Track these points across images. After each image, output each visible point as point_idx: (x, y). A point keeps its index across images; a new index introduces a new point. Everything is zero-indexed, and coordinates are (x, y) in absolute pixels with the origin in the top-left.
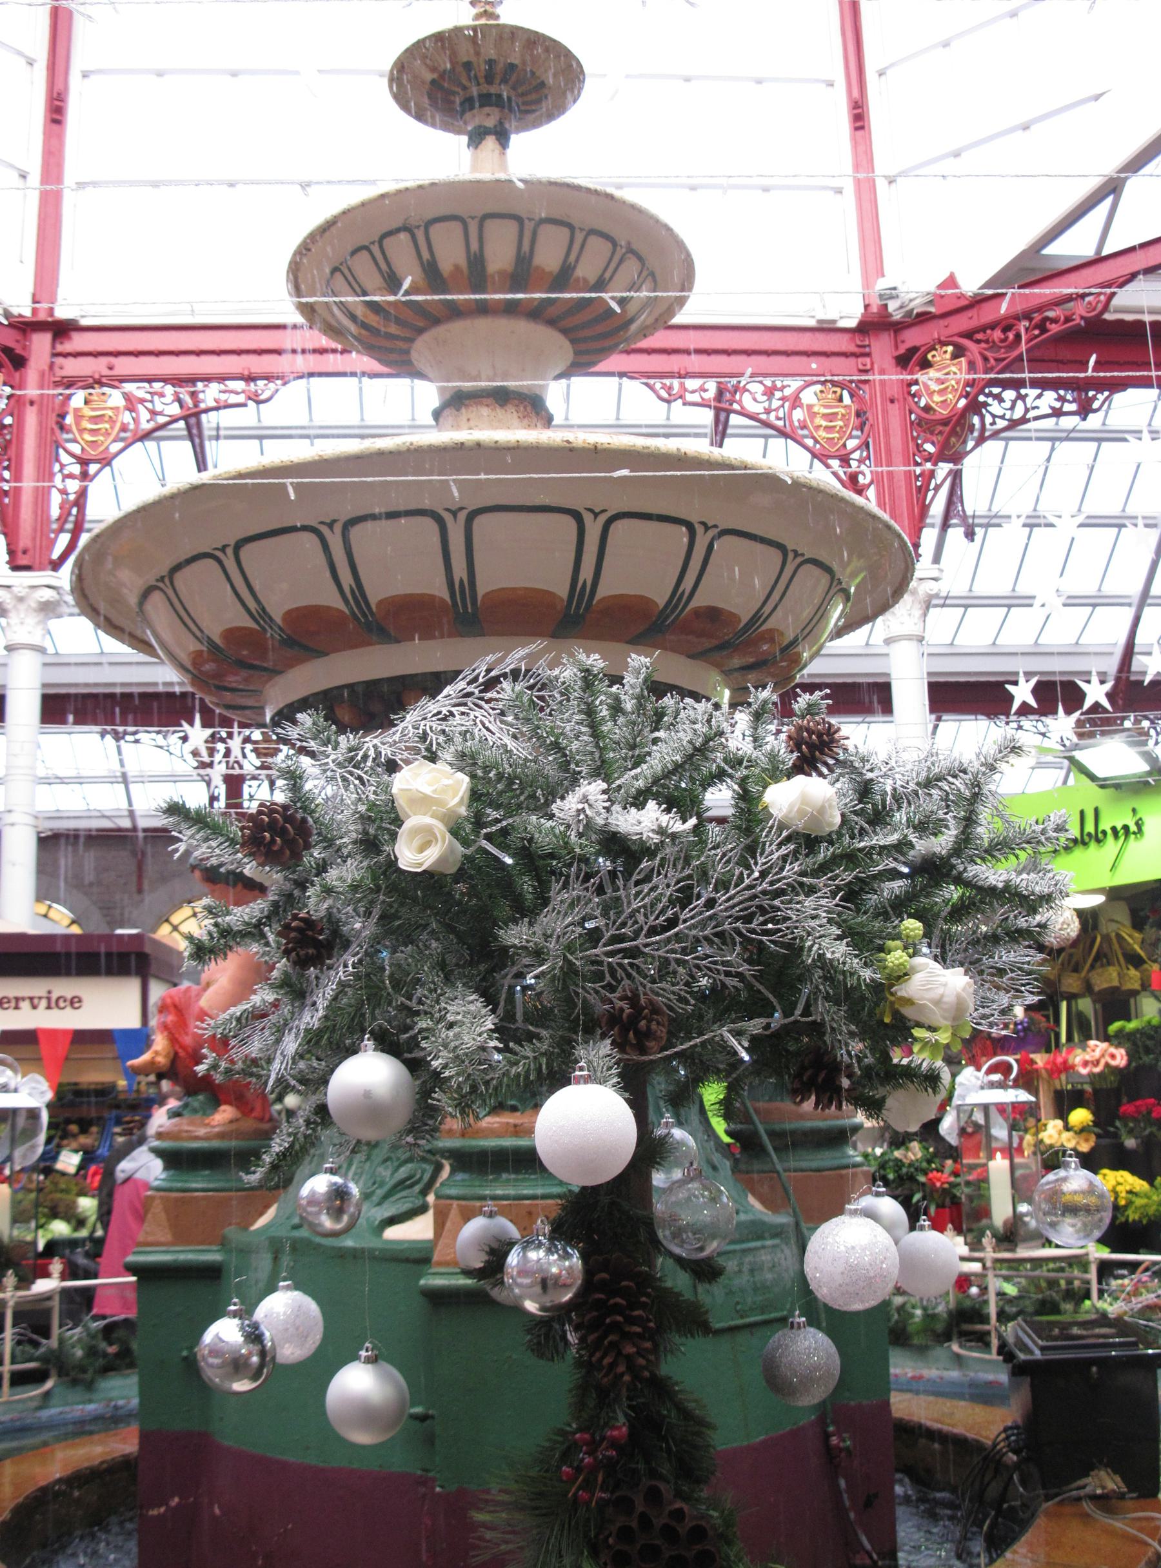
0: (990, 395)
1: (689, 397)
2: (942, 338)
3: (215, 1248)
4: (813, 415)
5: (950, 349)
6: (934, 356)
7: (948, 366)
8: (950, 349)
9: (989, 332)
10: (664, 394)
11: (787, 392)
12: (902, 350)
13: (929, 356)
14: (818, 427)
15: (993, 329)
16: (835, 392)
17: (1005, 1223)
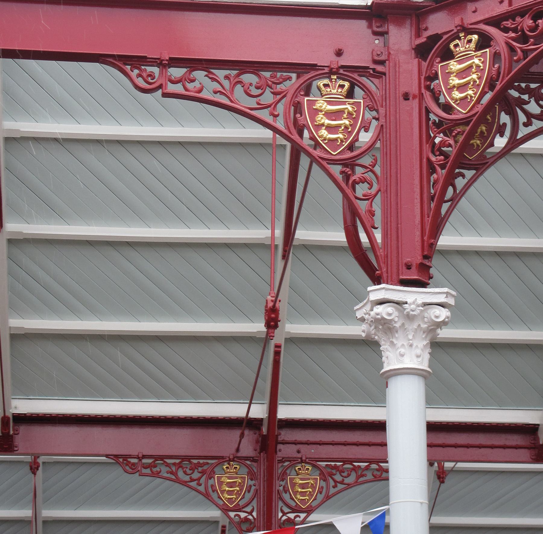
0: (527, 91)
1: (172, 88)
5: (475, 37)
6: (456, 46)
7: (472, 57)
8: (475, 37)
9: (518, 19)
10: (140, 82)
12: (422, 40)
14: (319, 127)
15: (522, 16)
16: (342, 86)
17: (355, 88)
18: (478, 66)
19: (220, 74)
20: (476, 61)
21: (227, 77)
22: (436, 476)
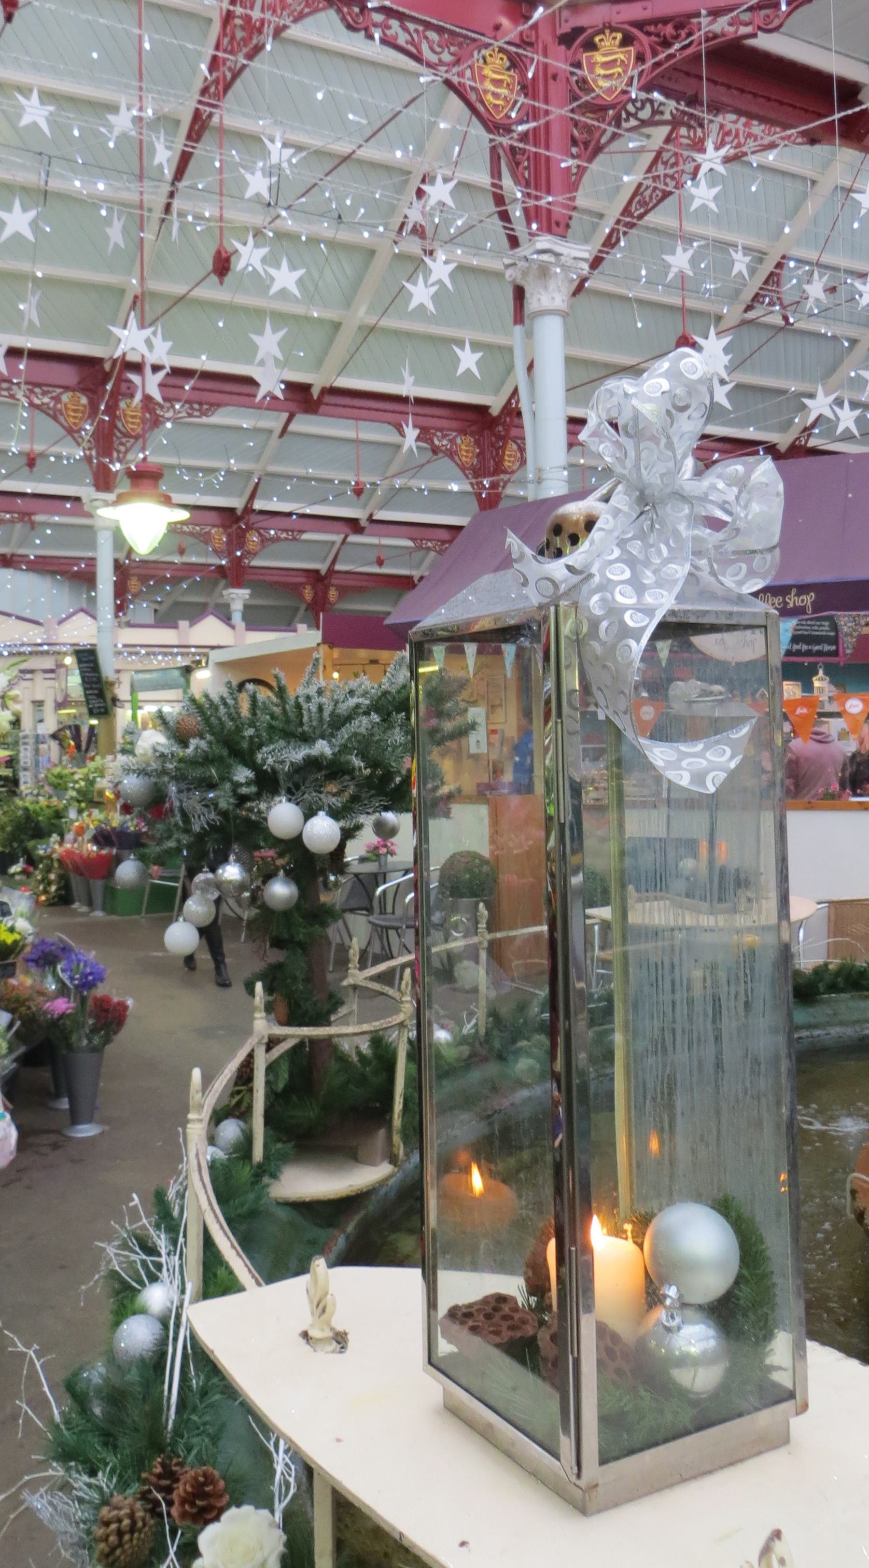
2: (613, 24)
3: (707, 938)
4: (66, 409)
8: (619, 36)
9: (660, 26)
11: (54, 394)
13: (597, 39)
18: (622, 61)
19: (411, 26)
20: (622, 57)
21: (416, 31)
22: (639, 1279)
